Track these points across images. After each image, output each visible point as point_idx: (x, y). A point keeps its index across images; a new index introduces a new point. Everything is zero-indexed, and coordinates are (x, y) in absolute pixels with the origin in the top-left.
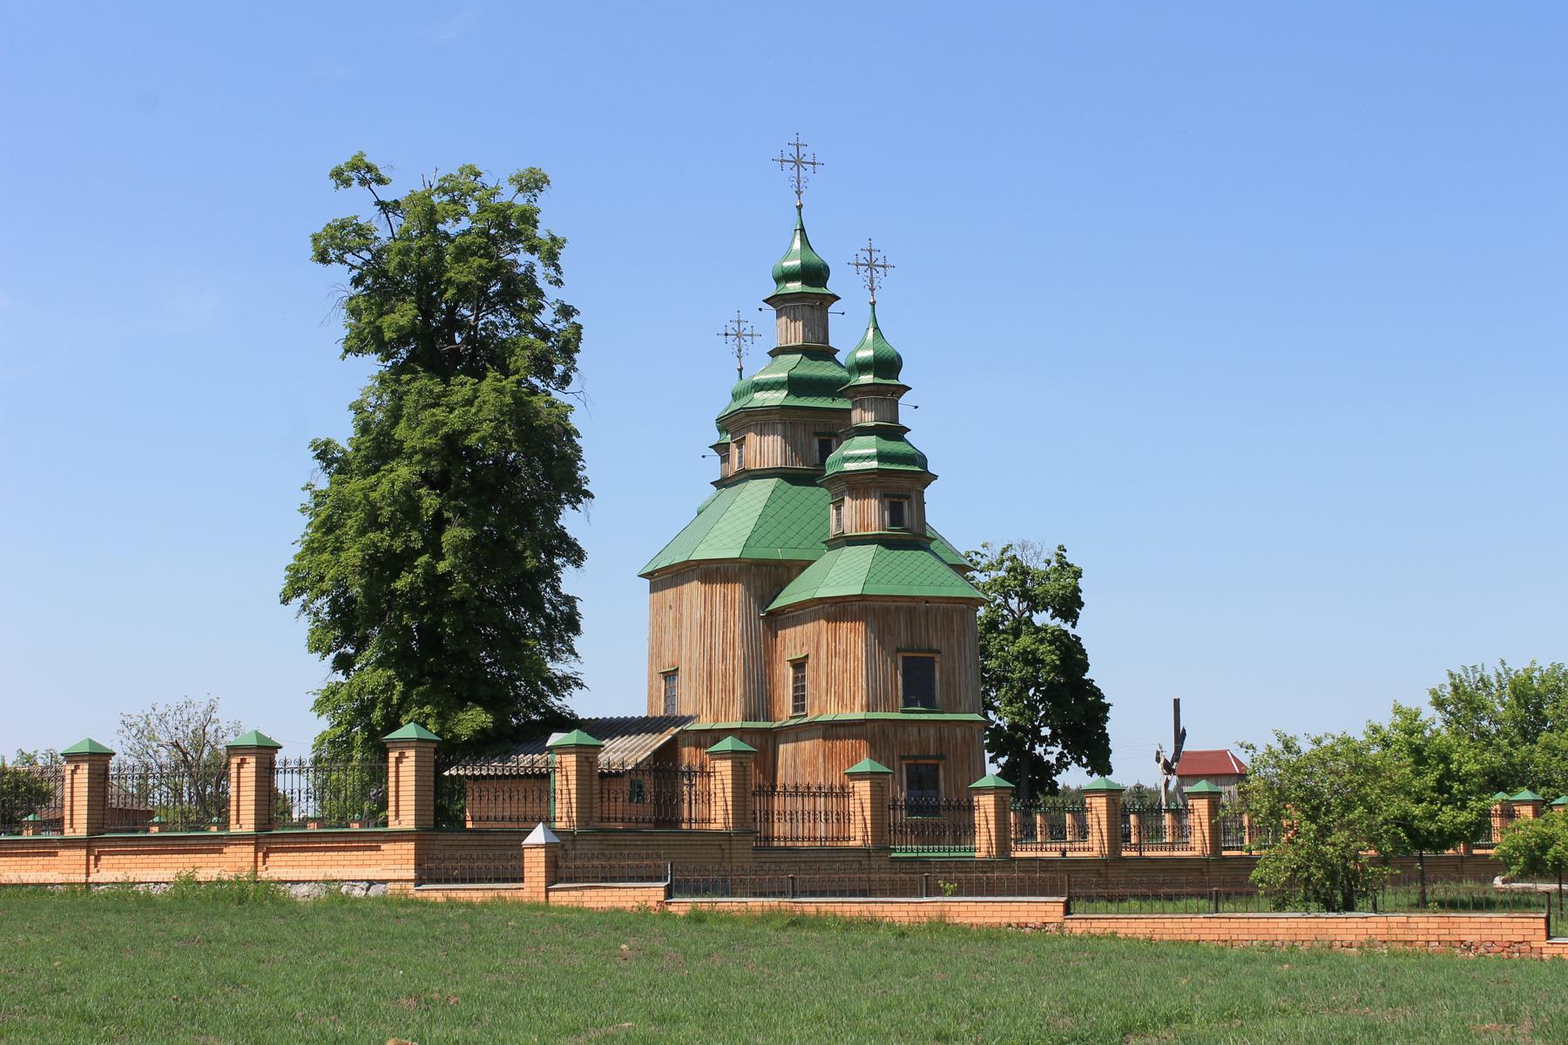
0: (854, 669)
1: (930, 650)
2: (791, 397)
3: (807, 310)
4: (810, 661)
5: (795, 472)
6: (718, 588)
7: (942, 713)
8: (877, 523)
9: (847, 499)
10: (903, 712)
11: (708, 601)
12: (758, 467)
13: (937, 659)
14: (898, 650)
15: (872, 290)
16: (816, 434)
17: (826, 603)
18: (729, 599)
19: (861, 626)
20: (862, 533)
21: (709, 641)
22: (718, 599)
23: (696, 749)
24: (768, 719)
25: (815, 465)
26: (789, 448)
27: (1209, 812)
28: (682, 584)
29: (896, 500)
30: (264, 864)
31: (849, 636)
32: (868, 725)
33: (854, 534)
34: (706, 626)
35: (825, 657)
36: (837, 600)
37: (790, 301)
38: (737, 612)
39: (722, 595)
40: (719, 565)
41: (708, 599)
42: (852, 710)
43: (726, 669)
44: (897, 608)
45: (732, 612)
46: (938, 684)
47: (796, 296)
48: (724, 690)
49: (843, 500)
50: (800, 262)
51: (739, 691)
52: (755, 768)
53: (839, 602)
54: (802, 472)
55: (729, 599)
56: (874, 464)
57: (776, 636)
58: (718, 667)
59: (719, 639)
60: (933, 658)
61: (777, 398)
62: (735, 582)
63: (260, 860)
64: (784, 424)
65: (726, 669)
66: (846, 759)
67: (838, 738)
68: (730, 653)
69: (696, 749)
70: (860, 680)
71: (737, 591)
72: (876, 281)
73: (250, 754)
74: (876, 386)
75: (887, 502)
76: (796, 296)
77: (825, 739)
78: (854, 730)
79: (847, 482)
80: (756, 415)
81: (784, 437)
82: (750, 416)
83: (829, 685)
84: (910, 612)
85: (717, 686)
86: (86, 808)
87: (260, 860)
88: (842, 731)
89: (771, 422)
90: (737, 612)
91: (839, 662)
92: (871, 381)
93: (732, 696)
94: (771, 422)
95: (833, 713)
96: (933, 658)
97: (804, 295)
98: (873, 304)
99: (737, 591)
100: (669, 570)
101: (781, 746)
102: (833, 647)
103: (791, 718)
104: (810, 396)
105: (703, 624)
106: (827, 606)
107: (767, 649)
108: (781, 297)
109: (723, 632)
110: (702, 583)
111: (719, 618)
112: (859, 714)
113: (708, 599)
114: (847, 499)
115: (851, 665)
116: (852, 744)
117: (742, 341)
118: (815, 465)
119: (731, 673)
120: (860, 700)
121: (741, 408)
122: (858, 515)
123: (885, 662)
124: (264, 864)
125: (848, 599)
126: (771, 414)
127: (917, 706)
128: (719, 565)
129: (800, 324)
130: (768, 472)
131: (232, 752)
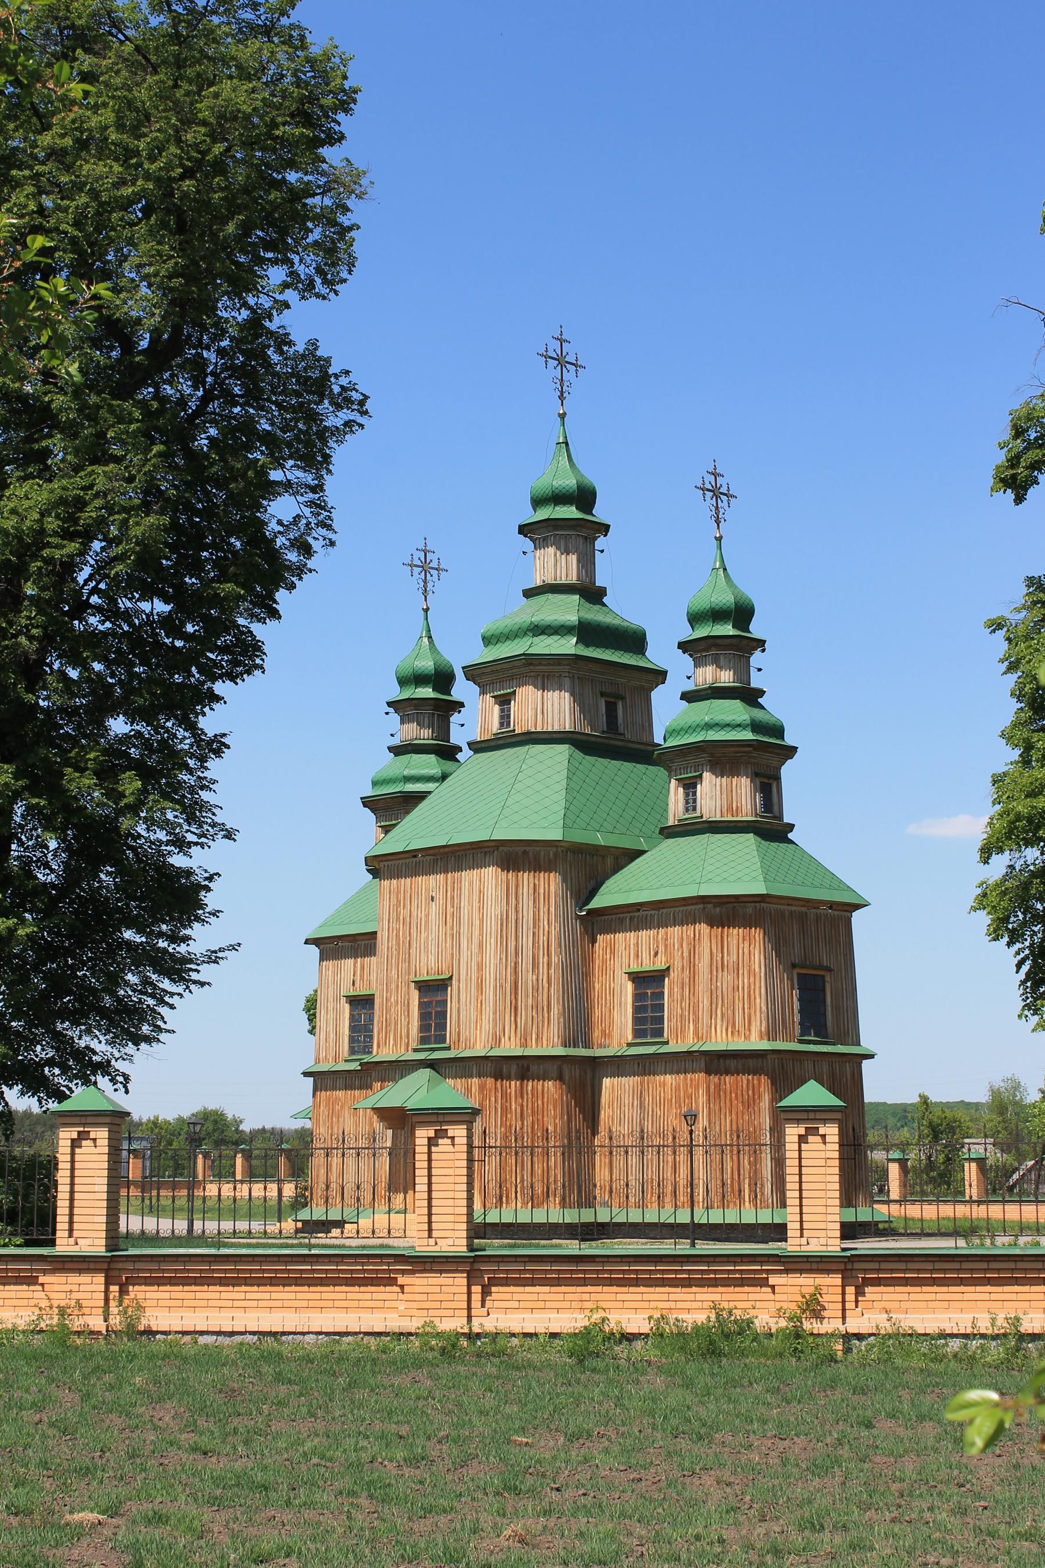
0: (749, 987)
1: (820, 967)
2: (581, 647)
3: (581, 541)
4: (672, 974)
5: (585, 738)
6: (526, 878)
7: (834, 1044)
8: (749, 807)
9: (707, 775)
10: (801, 1042)
11: (511, 894)
12: (539, 729)
13: (828, 978)
14: (794, 966)
15: (718, 522)
16: (602, 694)
17: (709, 903)
18: (542, 891)
19: (757, 934)
20: (730, 818)
21: (514, 943)
22: (526, 890)
23: (496, 1080)
24: (587, 1045)
25: (603, 732)
26: (577, 708)
27: (841, 1151)
28: (460, 869)
29: (766, 781)
30: (483, 1306)
31: (741, 946)
32: (769, 1057)
33: (718, 818)
34: (509, 924)
35: (707, 970)
36: (727, 900)
37: (562, 528)
38: (552, 909)
39: (532, 885)
40: (527, 849)
41: (512, 890)
42: (747, 1038)
43: (537, 980)
44: (791, 912)
45: (546, 909)
46: (829, 1009)
47: (573, 522)
48: (536, 1006)
49: (700, 776)
50: (574, 482)
51: (555, 1010)
52: (575, 1107)
53: (728, 903)
54: (593, 739)
55: (542, 891)
56: (748, 735)
57: (594, 941)
58: (528, 978)
59: (527, 941)
60: (823, 976)
61: (568, 645)
62: (549, 870)
63: (476, 1298)
64: (572, 678)
65: (537, 980)
66: (740, 1099)
67: (727, 1072)
68: (543, 960)
69: (496, 1080)
70: (758, 1000)
71: (552, 883)
72: (722, 511)
73: (825, 1121)
74: (738, 640)
75: (758, 781)
76: (573, 522)
77: (708, 1072)
78: (751, 1062)
79: (712, 755)
80: (540, 664)
81: (572, 694)
82: (531, 664)
83: (714, 1006)
84: (802, 918)
85: (525, 1001)
86: (105, 1204)
87: (476, 1298)
88: (732, 1063)
89: (557, 675)
90: (552, 909)
91: (726, 979)
92: (572, 651)
93: (546, 1015)
94: (557, 675)
95: (720, 1041)
96: (823, 976)
97: (582, 522)
98: (719, 539)
99: (552, 883)
100: (432, 852)
101: (607, 1082)
102: (719, 959)
103: (629, 1045)
104: (598, 647)
105: (504, 921)
106: (710, 906)
107: (584, 959)
108: (553, 523)
109: (534, 933)
110: (503, 870)
111: (528, 915)
112: (756, 1042)
113: (512, 890)
114: (707, 775)
115: (744, 980)
116: (748, 1080)
117: (428, 575)
118: (603, 732)
119: (546, 985)
120: (758, 1025)
121: (523, 654)
122: (724, 796)
123: (782, 981)
124: (483, 1306)
125: (741, 899)
126: (559, 664)
127: (810, 1035)
128: (527, 849)
129: (573, 558)
130: (554, 736)
131: (783, 1116)
